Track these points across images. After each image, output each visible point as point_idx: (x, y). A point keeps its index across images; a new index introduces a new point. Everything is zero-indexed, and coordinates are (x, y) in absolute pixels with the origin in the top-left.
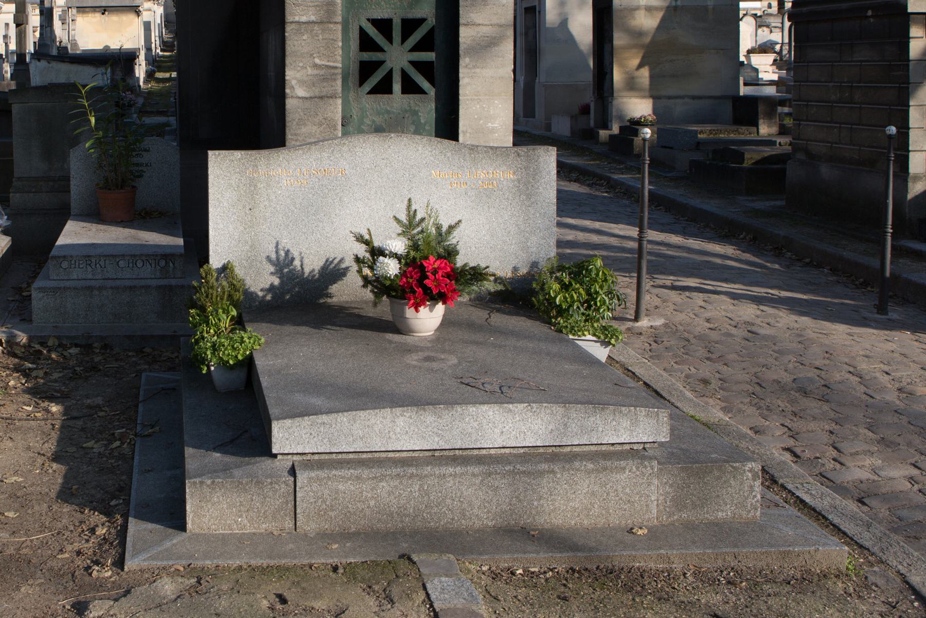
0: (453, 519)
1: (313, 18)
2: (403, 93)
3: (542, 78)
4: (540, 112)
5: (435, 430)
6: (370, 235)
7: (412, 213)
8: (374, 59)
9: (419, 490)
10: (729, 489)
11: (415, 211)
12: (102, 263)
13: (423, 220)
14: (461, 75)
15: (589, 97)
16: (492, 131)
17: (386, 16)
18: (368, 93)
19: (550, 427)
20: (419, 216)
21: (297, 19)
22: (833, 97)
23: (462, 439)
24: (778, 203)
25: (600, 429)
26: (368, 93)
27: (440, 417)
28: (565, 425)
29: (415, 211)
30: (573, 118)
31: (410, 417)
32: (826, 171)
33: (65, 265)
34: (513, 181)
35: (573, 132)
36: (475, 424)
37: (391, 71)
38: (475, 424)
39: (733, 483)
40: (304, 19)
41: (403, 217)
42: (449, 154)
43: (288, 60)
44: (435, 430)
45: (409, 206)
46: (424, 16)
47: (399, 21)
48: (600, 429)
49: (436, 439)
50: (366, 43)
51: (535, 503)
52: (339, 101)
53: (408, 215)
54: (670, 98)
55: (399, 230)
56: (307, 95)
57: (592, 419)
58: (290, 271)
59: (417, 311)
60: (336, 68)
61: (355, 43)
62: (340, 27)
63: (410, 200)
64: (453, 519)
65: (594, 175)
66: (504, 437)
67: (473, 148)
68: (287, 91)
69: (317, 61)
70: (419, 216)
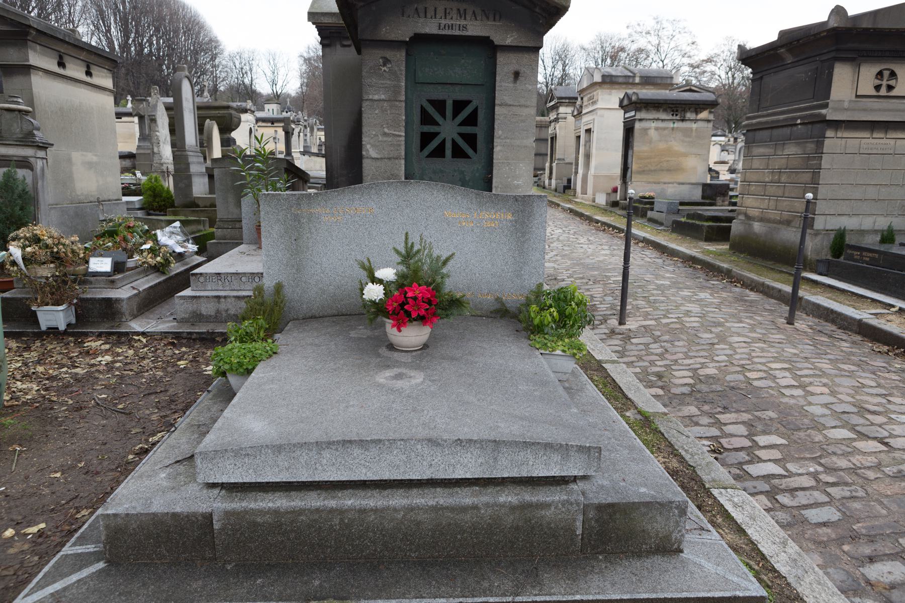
0: (375, 550)
1: (383, 97)
2: (453, 157)
3: (592, 171)
4: (590, 190)
5: (363, 462)
6: (369, 261)
7: (410, 244)
8: (432, 131)
9: (340, 524)
10: (655, 524)
11: (413, 243)
12: (229, 279)
13: (418, 251)
14: (495, 144)
15: (618, 183)
16: (518, 187)
17: (441, 98)
18: (427, 157)
19: (480, 461)
20: (416, 249)
21: (371, 97)
22: (767, 180)
23: (390, 471)
24: (724, 247)
25: (531, 463)
26: (427, 157)
27: (367, 450)
28: (495, 459)
29: (413, 243)
30: (608, 194)
31: (337, 450)
32: (757, 227)
33: (202, 279)
34: (511, 221)
35: (607, 204)
36: (404, 457)
37: (444, 141)
38: (404, 457)
39: (659, 518)
40: (376, 97)
41: (401, 248)
42: (459, 198)
43: (364, 130)
44: (363, 462)
45: (407, 239)
46: (470, 99)
47: (451, 102)
48: (531, 463)
49: (364, 471)
50: (426, 118)
51: (459, 536)
52: (403, 162)
53: (406, 247)
54: (665, 183)
55: (399, 259)
56: (379, 156)
57: (522, 454)
58: (35, 311)
59: (400, 331)
60: (400, 136)
61: (417, 118)
62: (403, 104)
63: (407, 233)
64: (375, 550)
65: (609, 226)
66: (432, 470)
67: (505, 199)
68: (364, 153)
69: (386, 130)
70: (416, 249)
